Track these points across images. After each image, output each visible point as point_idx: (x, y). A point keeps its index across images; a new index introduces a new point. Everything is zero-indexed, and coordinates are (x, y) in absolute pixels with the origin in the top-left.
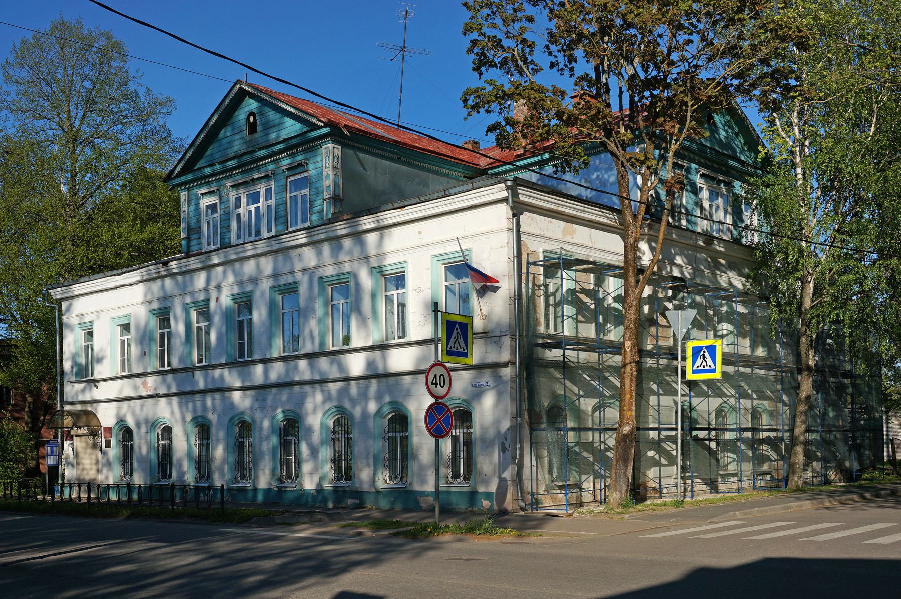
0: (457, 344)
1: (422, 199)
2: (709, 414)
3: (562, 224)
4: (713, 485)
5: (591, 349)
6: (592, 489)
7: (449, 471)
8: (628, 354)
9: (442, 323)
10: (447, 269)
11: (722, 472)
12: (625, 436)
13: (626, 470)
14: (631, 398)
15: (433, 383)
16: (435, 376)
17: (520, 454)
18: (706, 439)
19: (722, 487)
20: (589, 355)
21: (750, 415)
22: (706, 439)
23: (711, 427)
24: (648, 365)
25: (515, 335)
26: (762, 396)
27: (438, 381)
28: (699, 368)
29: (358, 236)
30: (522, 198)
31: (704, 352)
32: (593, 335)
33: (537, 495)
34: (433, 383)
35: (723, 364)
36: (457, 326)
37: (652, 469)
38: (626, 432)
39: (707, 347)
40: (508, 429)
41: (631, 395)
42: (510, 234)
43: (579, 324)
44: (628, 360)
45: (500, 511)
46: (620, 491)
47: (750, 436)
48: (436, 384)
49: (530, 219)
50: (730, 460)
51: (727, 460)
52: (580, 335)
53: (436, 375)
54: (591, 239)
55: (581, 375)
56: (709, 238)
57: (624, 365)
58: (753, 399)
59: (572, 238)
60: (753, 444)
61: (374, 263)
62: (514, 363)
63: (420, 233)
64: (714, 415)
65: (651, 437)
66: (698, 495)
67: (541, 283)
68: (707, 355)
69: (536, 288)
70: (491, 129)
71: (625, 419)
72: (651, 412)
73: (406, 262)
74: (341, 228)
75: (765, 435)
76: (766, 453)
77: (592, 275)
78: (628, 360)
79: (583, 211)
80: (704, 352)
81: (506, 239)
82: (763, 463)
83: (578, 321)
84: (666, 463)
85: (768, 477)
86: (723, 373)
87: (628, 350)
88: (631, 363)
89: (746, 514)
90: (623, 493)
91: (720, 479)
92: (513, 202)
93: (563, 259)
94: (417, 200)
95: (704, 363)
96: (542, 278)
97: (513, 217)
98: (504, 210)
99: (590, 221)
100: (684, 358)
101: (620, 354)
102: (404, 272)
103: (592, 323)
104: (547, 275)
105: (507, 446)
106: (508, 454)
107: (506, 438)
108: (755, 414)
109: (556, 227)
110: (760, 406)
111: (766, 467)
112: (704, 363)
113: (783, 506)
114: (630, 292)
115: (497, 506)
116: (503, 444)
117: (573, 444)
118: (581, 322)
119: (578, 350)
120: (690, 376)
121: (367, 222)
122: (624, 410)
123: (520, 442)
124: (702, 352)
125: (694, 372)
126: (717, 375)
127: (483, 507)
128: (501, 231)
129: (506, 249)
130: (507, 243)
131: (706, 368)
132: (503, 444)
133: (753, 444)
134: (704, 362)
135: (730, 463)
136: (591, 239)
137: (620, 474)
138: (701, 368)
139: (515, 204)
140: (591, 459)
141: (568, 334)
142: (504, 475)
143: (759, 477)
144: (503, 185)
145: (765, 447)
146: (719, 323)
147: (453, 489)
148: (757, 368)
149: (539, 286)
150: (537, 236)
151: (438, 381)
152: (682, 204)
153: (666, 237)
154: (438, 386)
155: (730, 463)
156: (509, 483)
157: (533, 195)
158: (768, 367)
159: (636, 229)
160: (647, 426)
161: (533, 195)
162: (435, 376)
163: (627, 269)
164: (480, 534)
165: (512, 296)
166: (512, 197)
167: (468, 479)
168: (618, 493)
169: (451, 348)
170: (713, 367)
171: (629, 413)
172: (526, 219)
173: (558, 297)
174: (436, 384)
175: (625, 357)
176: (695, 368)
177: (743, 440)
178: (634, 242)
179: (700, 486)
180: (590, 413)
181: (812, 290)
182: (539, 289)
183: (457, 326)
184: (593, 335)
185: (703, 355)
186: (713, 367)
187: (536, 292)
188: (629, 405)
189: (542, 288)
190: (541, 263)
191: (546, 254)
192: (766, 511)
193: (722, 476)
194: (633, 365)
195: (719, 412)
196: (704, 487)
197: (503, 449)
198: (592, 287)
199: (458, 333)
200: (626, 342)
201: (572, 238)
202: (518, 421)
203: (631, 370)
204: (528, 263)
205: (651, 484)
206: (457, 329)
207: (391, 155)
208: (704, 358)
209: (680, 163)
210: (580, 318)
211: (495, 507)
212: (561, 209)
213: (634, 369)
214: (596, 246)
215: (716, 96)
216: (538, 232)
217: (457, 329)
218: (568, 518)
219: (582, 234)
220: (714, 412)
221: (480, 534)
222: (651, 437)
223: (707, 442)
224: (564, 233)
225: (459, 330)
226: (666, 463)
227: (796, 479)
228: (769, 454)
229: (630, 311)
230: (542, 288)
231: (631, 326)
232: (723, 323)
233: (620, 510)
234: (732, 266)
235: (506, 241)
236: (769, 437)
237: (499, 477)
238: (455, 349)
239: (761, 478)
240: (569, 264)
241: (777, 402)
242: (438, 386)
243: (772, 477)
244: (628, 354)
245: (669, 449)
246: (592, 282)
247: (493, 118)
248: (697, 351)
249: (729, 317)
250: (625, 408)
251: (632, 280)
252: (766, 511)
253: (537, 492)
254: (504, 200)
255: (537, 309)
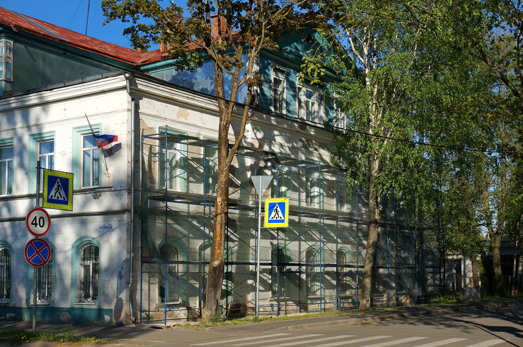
0: (58, 194)
1: (67, 84)
2: (300, 253)
3: (177, 108)
4: (303, 306)
5: (197, 203)
6: (198, 307)
7: (82, 293)
8: (219, 207)
9: (44, 178)
10: (85, 138)
11: (310, 297)
12: (215, 268)
13: (216, 294)
14: (221, 240)
15: (32, 224)
16: (35, 218)
17: (132, 280)
18: (297, 272)
19: (311, 307)
20: (199, 208)
21: (335, 256)
22: (297, 272)
23: (302, 263)
24: (250, 216)
25: (131, 190)
26: (346, 241)
27: (38, 222)
28: (273, 219)
29: (25, 109)
30: (140, 87)
31: (277, 207)
32: (202, 192)
33: (149, 311)
34: (32, 224)
35: (290, 214)
36: (58, 180)
37: (251, 293)
38: (215, 266)
39: (279, 204)
40: (124, 262)
41: (221, 238)
42: (129, 113)
43: (190, 184)
44: (219, 212)
45: (117, 323)
46: (211, 310)
47: (335, 270)
48: (36, 224)
49: (148, 103)
50: (318, 288)
51: (316, 288)
52: (190, 192)
53: (36, 218)
54: (202, 120)
55: (191, 222)
56: (303, 124)
57: (216, 215)
58: (337, 243)
59: (186, 119)
60: (337, 275)
61: (34, 131)
62: (129, 211)
63: (65, 110)
64: (304, 254)
65: (250, 269)
66: (290, 313)
67: (157, 151)
68: (279, 209)
69: (152, 155)
70: (127, 32)
71: (216, 255)
72: (251, 251)
73: (54, 132)
74: (13, 103)
75: (347, 270)
76: (348, 283)
77: (202, 149)
78: (219, 212)
79: (188, 98)
80: (277, 207)
81: (127, 118)
82: (346, 290)
83: (189, 182)
84: (264, 289)
85: (350, 301)
86: (291, 222)
87: (219, 204)
88: (221, 214)
89: (297, 328)
90: (213, 311)
91: (309, 302)
92: (131, 89)
93: (168, 134)
94: (63, 85)
95: (277, 216)
96: (157, 148)
97: (132, 101)
98: (124, 97)
99: (202, 107)
100: (263, 211)
101: (213, 206)
102: (53, 139)
103: (201, 183)
104: (162, 146)
105: (123, 274)
106: (124, 280)
107: (122, 268)
108: (340, 253)
109: (172, 111)
110: (344, 248)
111: (348, 293)
112: (277, 216)
113: (331, 322)
114: (222, 161)
115: (115, 320)
116: (120, 272)
117: (182, 274)
118: (192, 182)
119: (189, 203)
120: (267, 225)
121: (33, 99)
122: (215, 249)
123: (133, 272)
124: (275, 208)
125: (270, 222)
126: (285, 225)
127: (104, 320)
128: (123, 111)
129: (126, 124)
130: (128, 120)
131: (278, 219)
132: (120, 272)
133: (337, 275)
134: (277, 214)
135: (318, 290)
136: (202, 120)
137: (211, 297)
138: (275, 219)
139: (132, 91)
140: (197, 286)
141: (180, 191)
142: (120, 296)
143: (342, 301)
144: (123, 76)
145: (348, 278)
146: (311, 187)
147: (85, 307)
148: (340, 221)
149: (155, 154)
150: (154, 116)
151: (38, 222)
152: (283, 98)
153: (241, 120)
154: (38, 226)
155: (318, 290)
156: (124, 302)
157: (150, 85)
158: (350, 220)
159: (228, 114)
160: (247, 261)
161: (150, 85)
162: (35, 218)
163: (221, 143)
164: (64, 341)
165: (130, 160)
166: (130, 85)
167: (95, 299)
168: (209, 311)
169: (52, 196)
170: (283, 218)
171: (219, 251)
172: (144, 103)
173: (174, 163)
174: (36, 224)
175: (217, 209)
176: (270, 219)
177: (328, 273)
178: (226, 124)
179: (292, 306)
180: (198, 250)
181: (377, 165)
182: (155, 156)
183: (58, 180)
184: (202, 192)
185: (276, 209)
186: (66, 200)
187: (152, 158)
188: (219, 245)
189: (158, 155)
190: (157, 136)
191: (161, 130)
192: (315, 326)
193: (310, 299)
194: (223, 215)
195: (310, 253)
196: (295, 307)
197: (120, 277)
198: (202, 157)
199: (59, 186)
200: (218, 198)
201: (186, 119)
202: (132, 256)
203: (221, 219)
204: (143, 136)
205: (250, 305)
206: (58, 182)
207: (58, 51)
208: (276, 212)
209: (281, 69)
210: (191, 179)
211: (114, 321)
212: (175, 97)
213: (223, 219)
214: (206, 126)
215: (284, 19)
216: (155, 113)
217: (58, 182)
218: (166, 329)
219: (194, 116)
220: (305, 253)
221: (64, 341)
222: (250, 269)
223: (298, 274)
224: (179, 115)
225: (60, 184)
226: (264, 289)
227: (365, 302)
228: (351, 284)
229: (222, 175)
230: (158, 155)
231: (222, 186)
232: (315, 188)
233: (210, 324)
234: (323, 146)
235: (127, 119)
236: (351, 272)
237: (117, 297)
238: (56, 198)
239: (344, 301)
240: (181, 137)
241: (358, 246)
242: (38, 226)
243: (353, 300)
244: (219, 207)
245: (265, 278)
246: (202, 153)
247: (128, 25)
248: (272, 206)
249: (319, 183)
250: (216, 247)
251: (224, 152)
252: (315, 326)
253: (149, 309)
254: (124, 88)
255: (153, 171)
